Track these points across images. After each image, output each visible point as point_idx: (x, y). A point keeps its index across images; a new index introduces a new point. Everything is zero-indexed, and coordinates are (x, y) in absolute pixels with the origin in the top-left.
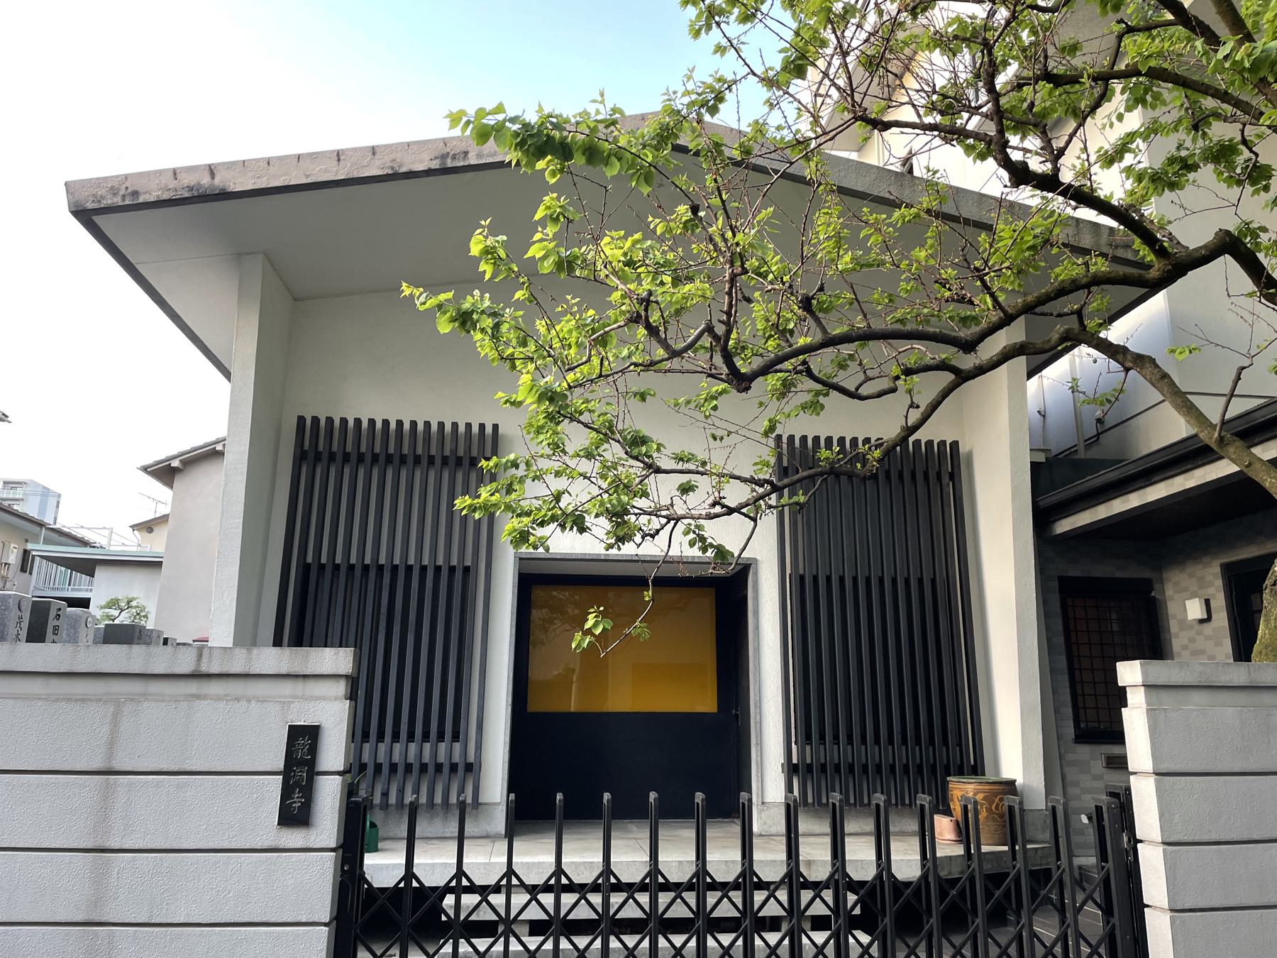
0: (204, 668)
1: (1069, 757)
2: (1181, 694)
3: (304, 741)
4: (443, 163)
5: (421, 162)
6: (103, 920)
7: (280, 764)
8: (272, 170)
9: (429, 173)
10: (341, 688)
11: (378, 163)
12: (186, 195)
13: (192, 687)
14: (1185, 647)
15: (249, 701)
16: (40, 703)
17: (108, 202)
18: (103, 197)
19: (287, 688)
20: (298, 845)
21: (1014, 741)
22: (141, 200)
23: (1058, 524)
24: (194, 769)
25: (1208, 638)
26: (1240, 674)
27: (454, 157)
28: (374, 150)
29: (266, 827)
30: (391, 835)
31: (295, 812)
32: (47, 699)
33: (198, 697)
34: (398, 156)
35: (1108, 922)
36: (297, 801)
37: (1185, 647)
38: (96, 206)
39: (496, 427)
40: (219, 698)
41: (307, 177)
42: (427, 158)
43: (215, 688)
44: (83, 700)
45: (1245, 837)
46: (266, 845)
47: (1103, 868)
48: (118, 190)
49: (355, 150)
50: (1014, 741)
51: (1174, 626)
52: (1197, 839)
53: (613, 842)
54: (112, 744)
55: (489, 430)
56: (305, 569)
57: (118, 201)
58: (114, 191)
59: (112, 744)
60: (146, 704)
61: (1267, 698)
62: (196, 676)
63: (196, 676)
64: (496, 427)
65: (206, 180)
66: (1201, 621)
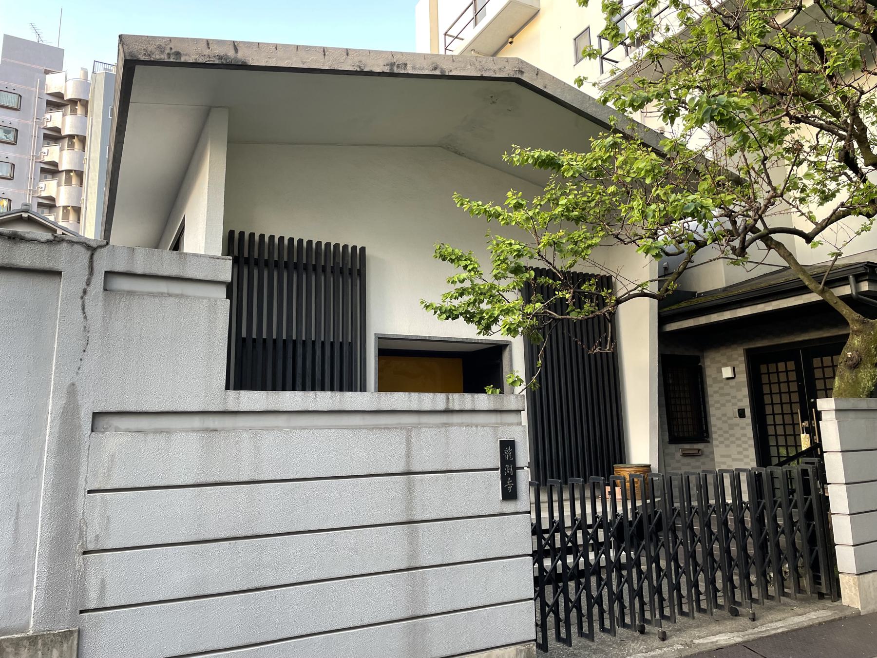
0: (451, 407)
1: (666, 451)
3: (507, 447)
4: (392, 69)
5: (378, 66)
6: (418, 565)
7: (498, 464)
8: (280, 53)
9: (380, 74)
11: (350, 61)
12: (217, 62)
13: (443, 419)
14: (716, 392)
15: (477, 426)
16: (364, 431)
17: (157, 56)
18: (152, 53)
19: (493, 419)
20: (512, 511)
21: (642, 444)
22: (183, 60)
23: (668, 325)
25: (732, 387)
27: (398, 66)
28: (347, 52)
31: (510, 493)
32: (438, 426)
34: (364, 59)
35: (809, 525)
37: (716, 392)
38: (147, 58)
41: (304, 63)
42: (382, 64)
44: (387, 428)
46: (496, 512)
47: (806, 500)
48: (165, 49)
49: (335, 49)
50: (642, 444)
51: (709, 381)
54: (408, 455)
57: (164, 57)
58: (161, 49)
59: (408, 455)
60: (423, 430)
61: (871, 415)
65: (231, 53)
66: (728, 379)
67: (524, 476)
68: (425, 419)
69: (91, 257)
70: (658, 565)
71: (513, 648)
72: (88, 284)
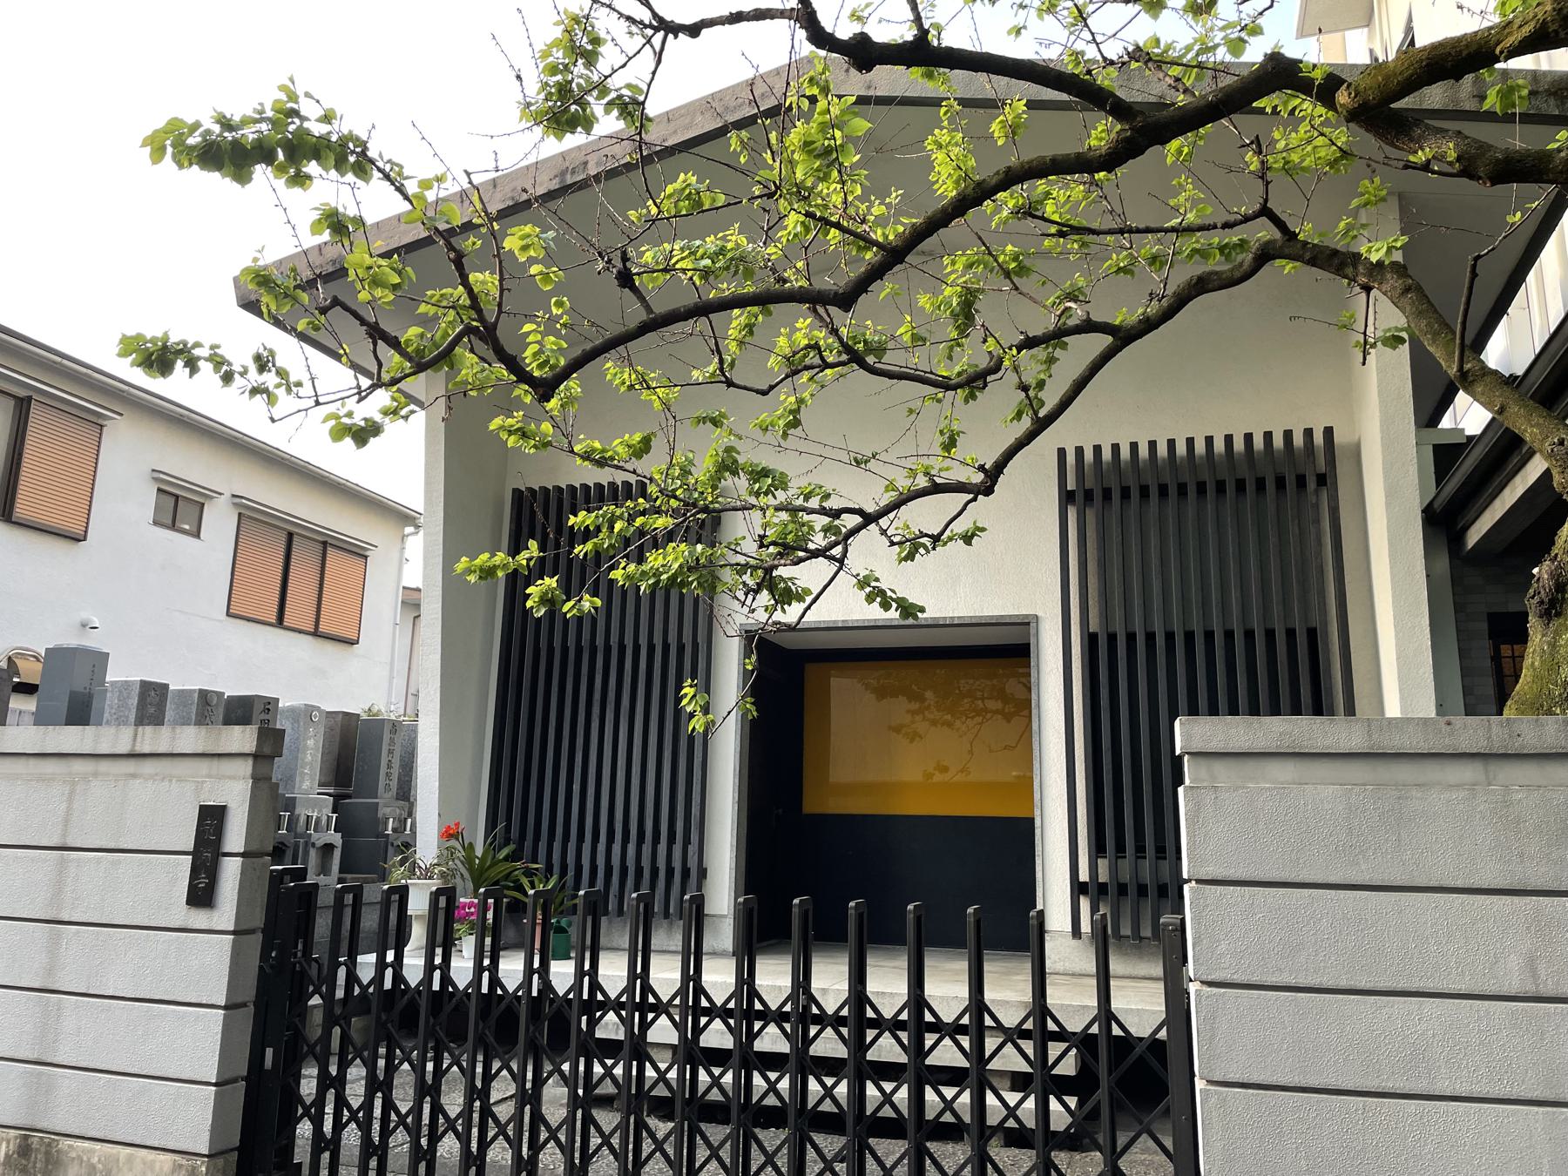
0: (139, 749)
2: (1250, 766)
3: (212, 819)
7: (190, 846)
10: (246, 767)
19: (203, 766)
24: (125, 846)
26: (1474, 732)
29: (181, 913)
30: (615, 945)
31: (201, 895)
33: (134, 776)
36: (203, 882)
39: (1329, 431)
40: (152, 777)
42: (546, 178)
43: (149, 767)
45: (1343, 983)
52: (1255, 979)
53: (869, 970)
55: (1319, 438)
56: (1091, 641)
62: (132, 756)
63: (132, 756)
64: (1329, 431)
67: (231, 872)
68: (104, 766)
69: (1266, 201)
70: (416, 1144)
71: (170, 1156)
72: (1215, 227)
